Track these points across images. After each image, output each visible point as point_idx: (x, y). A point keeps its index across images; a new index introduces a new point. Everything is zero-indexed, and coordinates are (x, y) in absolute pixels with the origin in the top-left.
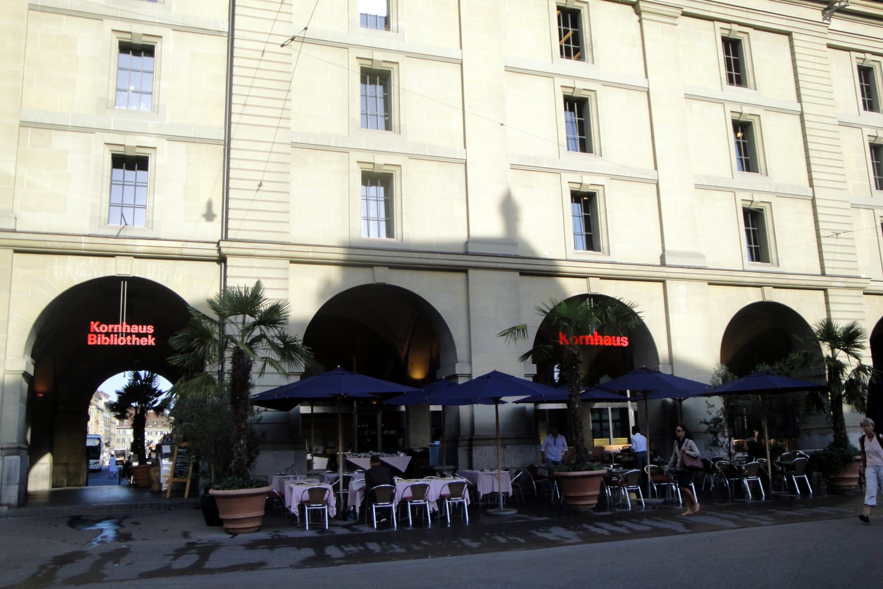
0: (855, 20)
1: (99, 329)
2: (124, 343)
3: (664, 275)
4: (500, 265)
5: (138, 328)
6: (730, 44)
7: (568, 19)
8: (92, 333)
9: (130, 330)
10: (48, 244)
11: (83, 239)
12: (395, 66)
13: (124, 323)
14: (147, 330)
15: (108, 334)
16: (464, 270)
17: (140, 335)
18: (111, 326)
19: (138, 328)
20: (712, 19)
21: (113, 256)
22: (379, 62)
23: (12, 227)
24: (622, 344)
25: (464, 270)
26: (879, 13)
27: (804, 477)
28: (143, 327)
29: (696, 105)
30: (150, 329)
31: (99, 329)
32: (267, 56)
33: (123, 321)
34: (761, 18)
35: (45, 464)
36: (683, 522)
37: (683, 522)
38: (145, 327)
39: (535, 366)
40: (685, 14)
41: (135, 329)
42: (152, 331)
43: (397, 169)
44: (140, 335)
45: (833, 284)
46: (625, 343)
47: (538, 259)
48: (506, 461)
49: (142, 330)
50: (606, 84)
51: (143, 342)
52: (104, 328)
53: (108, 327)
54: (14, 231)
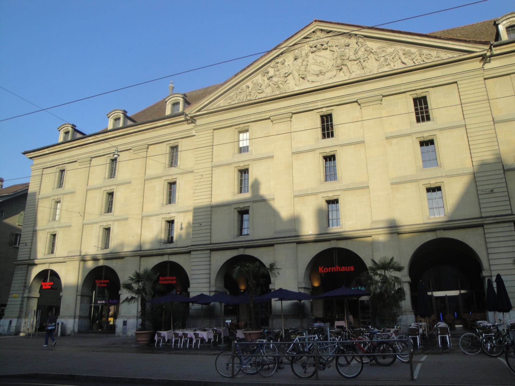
0: (462, 63)
1: (323, 271)
2: (168, 283)
3: (371, 234)
4: (286, 241)
5: (345, 268)
6: (422, 99)
7: (417, 103)
8: (160, 280)
9: (341, 269)
10: (147, 254)
11: (109, 255)
12: (435, 137)
13: (337, 266)
14: (350, 269)
15: (164, 280)
16: (482, 225)
17: (172, 280)
18: (330, 268)
19: (345, 268)
20: (312, 110)
21: (45, 264)
22: (427, 137)
23: (55, 257)
24: (351, 270)
25: (482, 225)
26: (449, 61)
27: (417, 338)
28: (348, 268)
29: (394, 141)
30: (175, 278)
31: (323, 271)
32: (204, 177)
33: (336, 265)
34: (433, 81)
35: (111, 323)
36: (352, 356)
37: (352, 356)
38: (349, 267)
39: (39, 295)
40: (384, 96)
41: (171, 278)
42: (175, 278)
43: (442, 184)
44: (172, 280)
45: (486, 222)
46: (352, 269)
47: (331, 234)
48: (287, 325)
49: (348, 269)
50: (441, 129)
51: (173, 282)
52: (163, 278)
53: (328, 269)
54: (55, 258)
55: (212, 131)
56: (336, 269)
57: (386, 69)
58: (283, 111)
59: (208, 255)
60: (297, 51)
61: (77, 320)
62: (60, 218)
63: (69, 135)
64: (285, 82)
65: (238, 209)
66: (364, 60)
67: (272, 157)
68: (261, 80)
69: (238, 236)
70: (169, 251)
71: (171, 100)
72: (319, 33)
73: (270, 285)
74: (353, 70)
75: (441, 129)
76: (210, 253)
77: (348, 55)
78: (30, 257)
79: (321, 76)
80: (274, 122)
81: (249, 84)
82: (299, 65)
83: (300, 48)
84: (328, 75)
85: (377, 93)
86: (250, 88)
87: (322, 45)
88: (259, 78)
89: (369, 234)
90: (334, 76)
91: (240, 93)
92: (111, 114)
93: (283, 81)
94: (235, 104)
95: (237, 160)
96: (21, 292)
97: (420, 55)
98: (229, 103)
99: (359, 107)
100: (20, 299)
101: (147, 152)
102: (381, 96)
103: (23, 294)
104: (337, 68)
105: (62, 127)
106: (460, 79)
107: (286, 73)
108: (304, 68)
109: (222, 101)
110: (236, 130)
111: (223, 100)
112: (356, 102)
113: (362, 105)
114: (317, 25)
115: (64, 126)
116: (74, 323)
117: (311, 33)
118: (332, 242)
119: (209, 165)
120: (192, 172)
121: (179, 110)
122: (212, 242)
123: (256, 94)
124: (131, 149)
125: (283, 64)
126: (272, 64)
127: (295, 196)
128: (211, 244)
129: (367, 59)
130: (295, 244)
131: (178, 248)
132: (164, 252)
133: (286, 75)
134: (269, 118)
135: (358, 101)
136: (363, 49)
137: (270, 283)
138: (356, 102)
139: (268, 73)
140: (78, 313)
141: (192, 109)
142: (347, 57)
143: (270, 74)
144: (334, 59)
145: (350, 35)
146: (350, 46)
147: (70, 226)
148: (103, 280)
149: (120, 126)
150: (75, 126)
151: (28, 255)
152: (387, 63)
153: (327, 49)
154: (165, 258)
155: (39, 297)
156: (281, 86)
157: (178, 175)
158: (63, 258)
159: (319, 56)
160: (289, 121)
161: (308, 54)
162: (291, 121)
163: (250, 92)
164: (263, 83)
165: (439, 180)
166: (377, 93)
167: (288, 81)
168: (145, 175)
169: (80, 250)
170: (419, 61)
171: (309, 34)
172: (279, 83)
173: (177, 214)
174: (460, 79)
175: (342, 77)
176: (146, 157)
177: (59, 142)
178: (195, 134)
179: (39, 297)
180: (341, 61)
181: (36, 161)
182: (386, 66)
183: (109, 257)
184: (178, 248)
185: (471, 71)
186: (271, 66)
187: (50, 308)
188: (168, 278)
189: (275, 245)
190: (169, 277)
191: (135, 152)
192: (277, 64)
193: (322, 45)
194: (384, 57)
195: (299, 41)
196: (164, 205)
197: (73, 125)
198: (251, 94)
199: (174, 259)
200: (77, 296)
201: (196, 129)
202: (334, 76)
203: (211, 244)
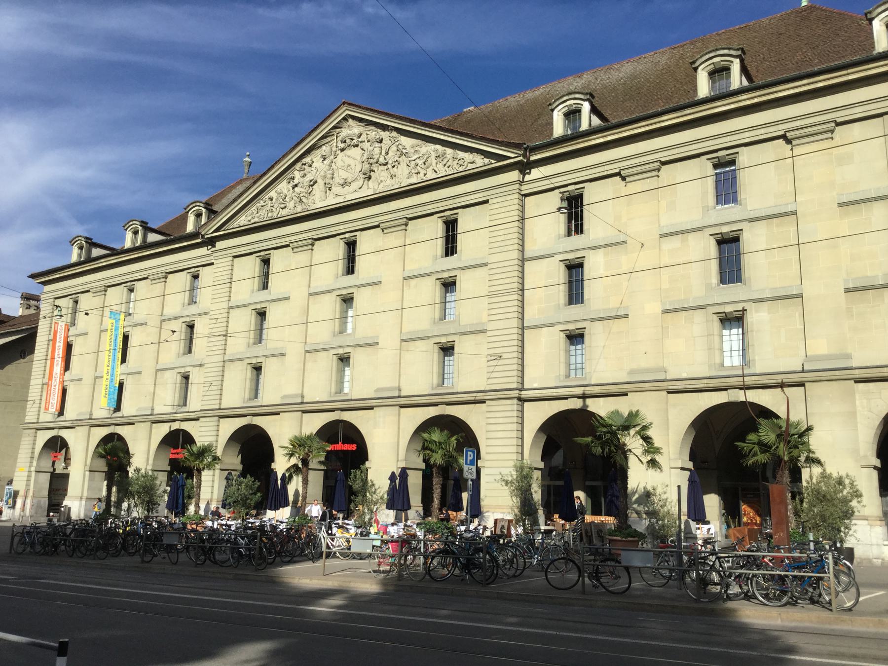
29: (413, 282)
32: (219, 321)
34: (463, 199)
50: (463, 268)
54: (65, 421)
55: (231, 258)
56: (340, 446)
57: (414, 180)
58: (304, 236)
59: (216, 423)
60: (324, 148)
61: (83, 502)
62: (354, 329)
63: (201, 218)
64: (310, 193)
65: (566, 332)
66: (393, 165)
67: (288, 298)
68: (286, 188)
69: (250, 399)
70: (179, 416)
71: (192, 210)
72: (351, 121)
73: (366, 462)
74: (382, 178)
75: (463, 268)
76: (219, 421)
77: (376, 157)
78: (38, 419)
79: (347, 187)
80: (385, 231)
81: (273, 194)
82: (325, 169)
83: (329, 142)
84: (355, 185)
85: (304, 236)
86: (274, 201)
87: (353, 139)
88: (283, 186)
89: (369, 405)
90: (360, 188)
91: (262, 206)
92: (127, 226)
93: (306, 193)
94: (255, 223)
95: (186, 313)
96: (28, 465)
97: (447, 165)
98: (250, 221)
99: (624, 183)
100: (26, 474)
101: (166, 282)
102: (833, 124)
103: (30, 467)
104: (364, 176)
105: (75, 240)
106: (491, 197)
107: (311, 181)
108: (330, 174)
109: (243, 217)
110: (125, 288)
111: (244, 216)
112: (784, 137)
113: (794, 143)
114: (347, 109)
115: (77, 239)
116: (80, 506)
117: (340, 121)
118: (177, 423)
119: (225, 305)
120: (485, 265)
121: (186, 231)
122: (222, 407)
123: (278, 209)
124: (147, 278)
125: (310, 166)
126: (298, 166)
127: (403, 341)
128: (220, 409)
129: (397, 163)
130: (398, 407)
131: (264, 406)
132: (176, 418)
133: (312, 183)
134: (378, 226)
135: (788, 134)
136: (394, 148)
137: (273, 461)
138: (618, 174)
139: (293, 178)
140: (85, 494)
141: (208, 228)
142: (375, 161)
143: (296, 181)
144: (363, 162)
145: (384, 128)
146: (383, 141)
147: (284, 355)
148: (340, 443)
149: (138, 245)
150: (147, 223)
151: (218, 402)
152: (417, 172)
153: (357, 146)
154: (175, 426)
155: (169, 470)
156: (304, 199)
157: (197, 316)
158: (71, 422)
159: (348, 157)
160: (403, 230)
161: (337, 153)
162: (406, 230)
163: (273, 206)
164: (287, 194)
165: (450, 339)
166: (402, 214)
167: (314, 192)
168: (309, 287)
169: (91, 411)
170: (455, 169)
171: (338, 123)
172: (301, 195)
173: (192, 368)
174: (491, 197)
175: (369, 190)
176: (793, 157)
177: (72, 262)
178: (213, 261)
179: (169, 470)
180: (369, 165)
181: (48, 288)
182: (414, 174)
183: (118, 422)
184: (264, 406)
185: (780, 122)
186: (298, 169)
187: (527, 491)
188: (179, 450)
189: (281, 414)
190: (343, 443)
191: (153, 282)
192: (304, 166)
193: (353, 139)
194: (414, 160)
195: (328, 133)
196: (181, 355)
197: (142, 222)
198: (273, 209)
199: (347, 416)
200: (85, 472)
201: (214, 255)
202: (360, 188)
203: (399, 397)
